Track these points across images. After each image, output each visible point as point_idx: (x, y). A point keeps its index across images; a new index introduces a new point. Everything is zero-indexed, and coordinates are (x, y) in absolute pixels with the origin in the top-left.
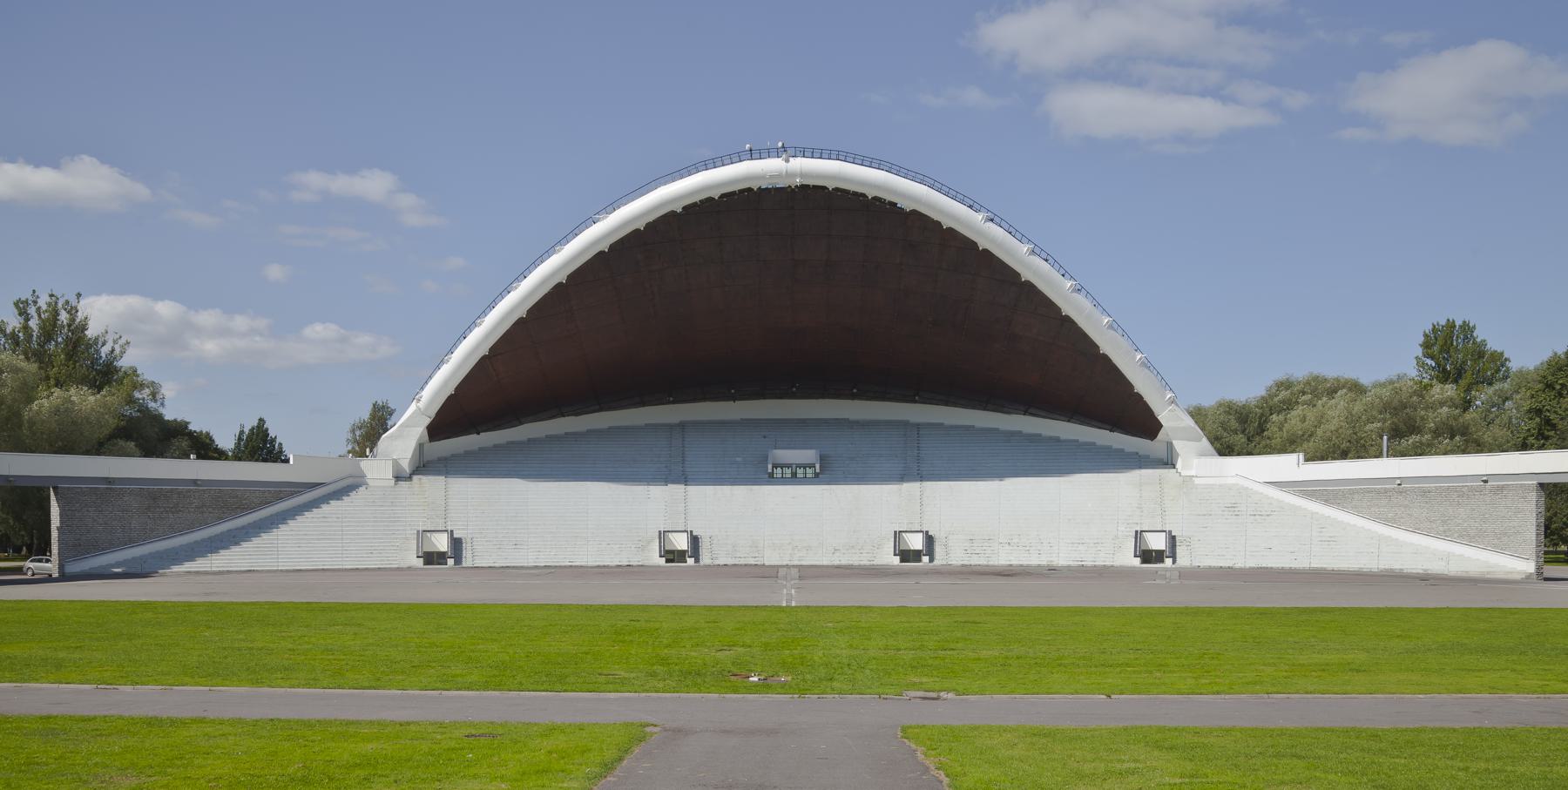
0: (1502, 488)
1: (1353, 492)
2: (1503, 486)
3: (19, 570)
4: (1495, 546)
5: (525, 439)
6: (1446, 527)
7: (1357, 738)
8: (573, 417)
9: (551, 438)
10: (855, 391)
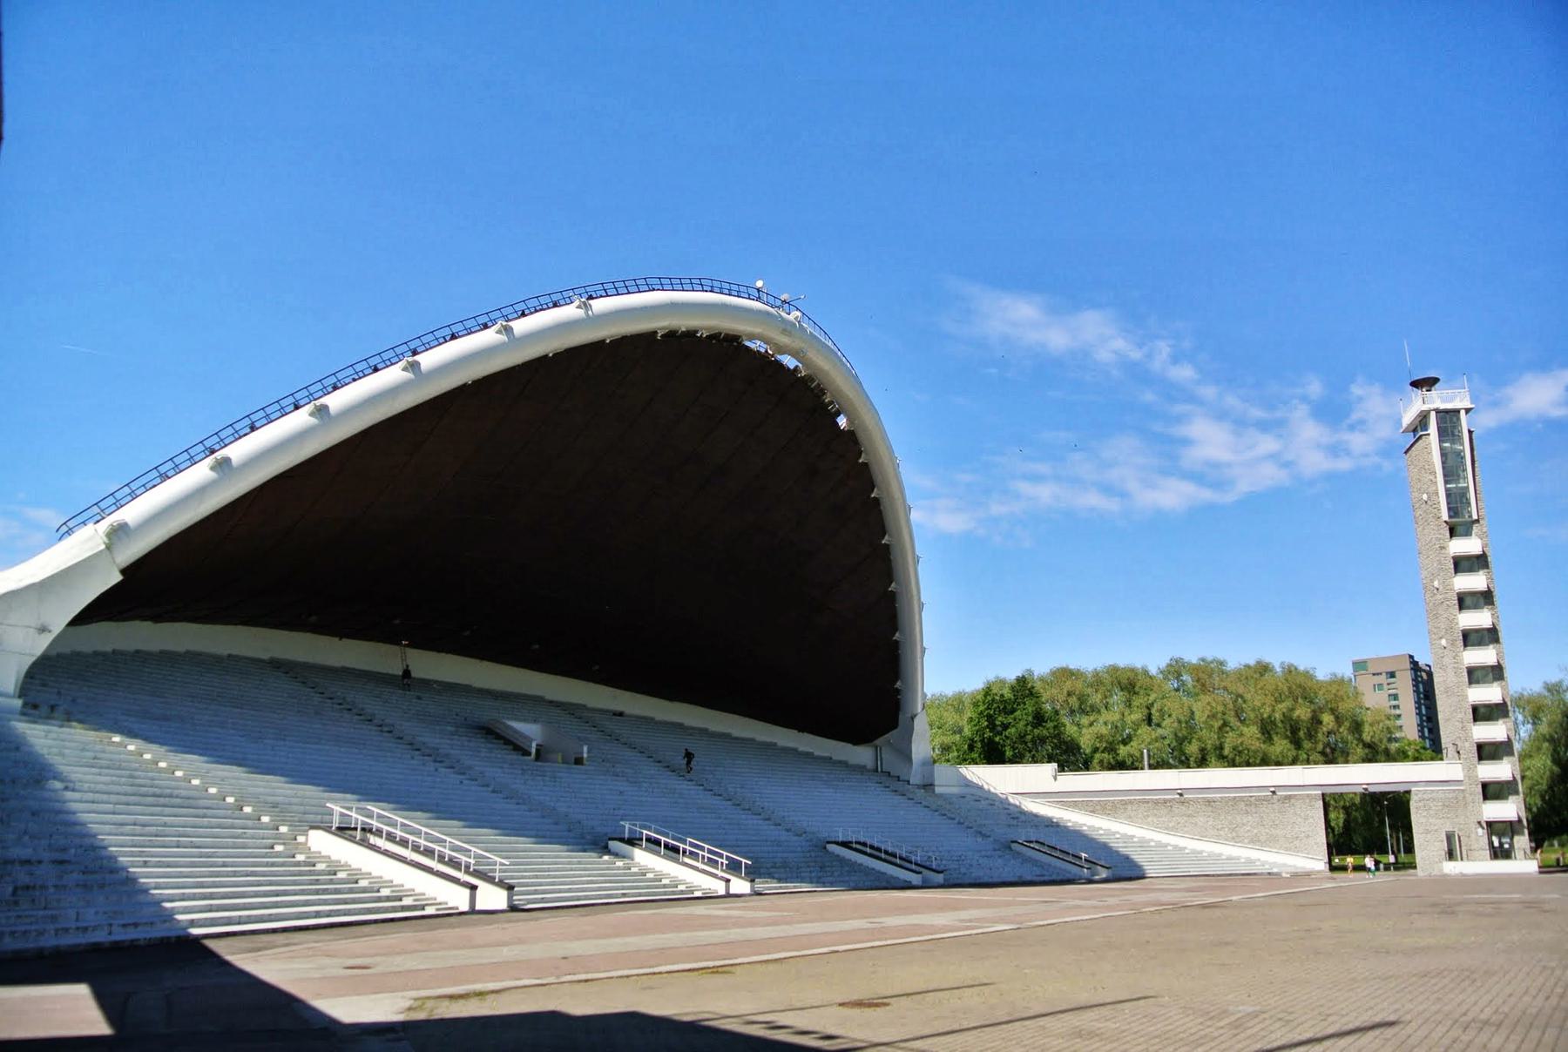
0: (1289, 798)
1: (1125, 803)
2: (1290, 796)
4: (1286, 849)
6: (1234, 834)
8: (148, 624)
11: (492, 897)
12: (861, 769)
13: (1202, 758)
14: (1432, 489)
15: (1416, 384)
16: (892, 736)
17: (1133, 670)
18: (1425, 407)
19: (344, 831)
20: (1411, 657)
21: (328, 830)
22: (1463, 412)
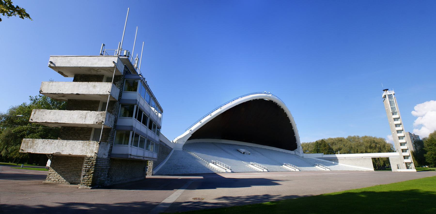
3: (123, 205)
5: (47, 93)
7: (304, 153)
9: (200, 143)
10: (225, 210)
11: (265, 170)
12: (293, 154)
13: (349, 151)
14: (388, 107)
15: (384, 90)
16: (297, 149)
17: (342, 138)
18: (385, 94)
19: (213, 163)
20: (409, 132)
21: (212, 163)
22: (393, 95)
